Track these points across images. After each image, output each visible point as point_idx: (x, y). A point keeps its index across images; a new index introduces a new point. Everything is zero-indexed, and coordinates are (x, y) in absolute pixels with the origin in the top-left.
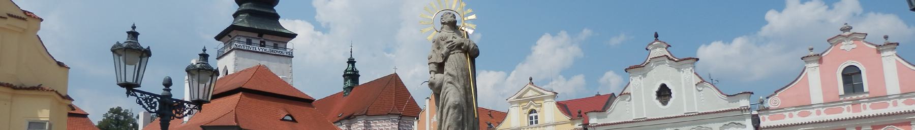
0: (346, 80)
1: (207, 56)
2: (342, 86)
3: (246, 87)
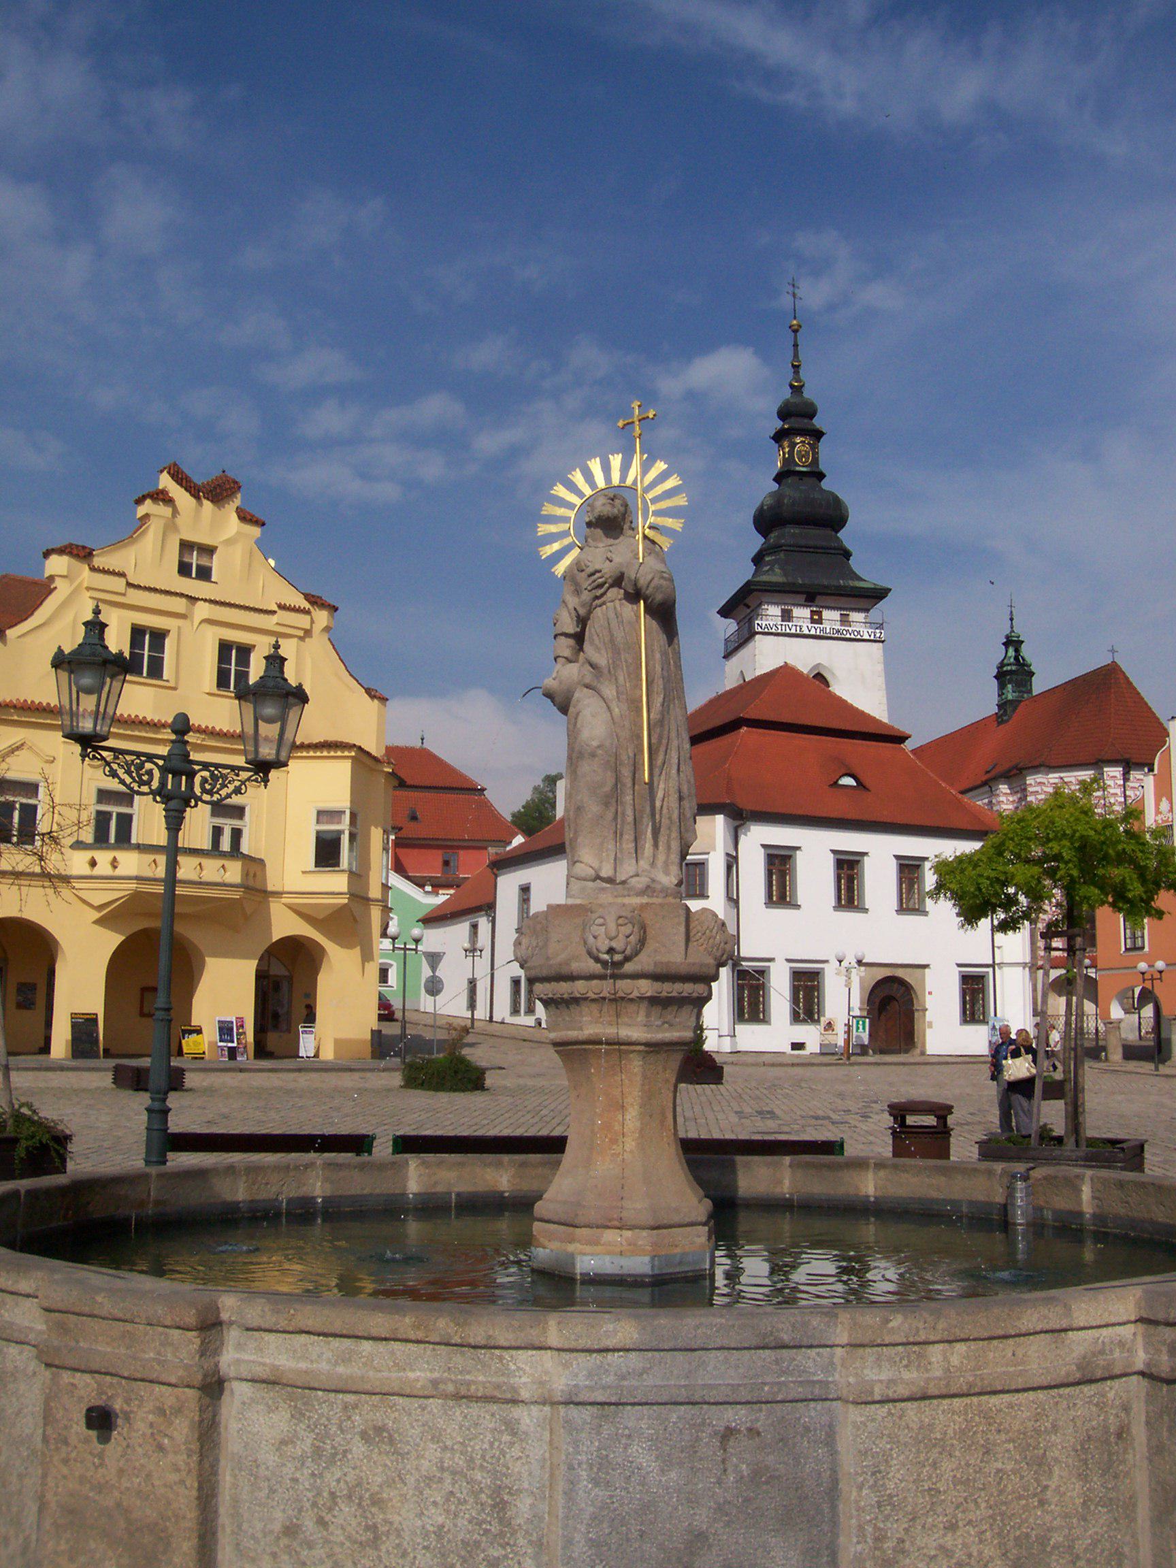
0: (1002, 686)
1: (283, 660)
2: (995, 700)
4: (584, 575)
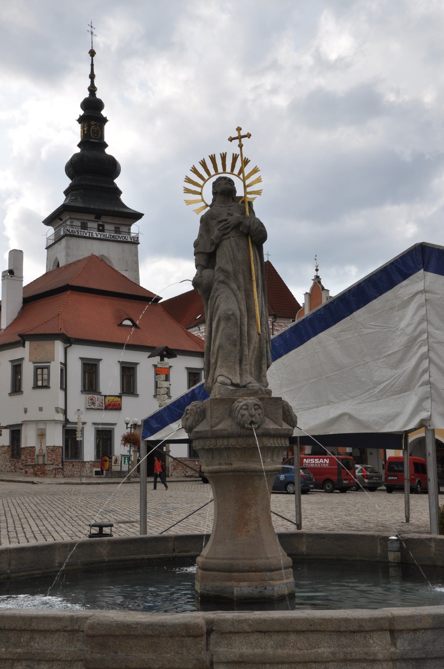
3: (75, 284)
4: (215, 222)
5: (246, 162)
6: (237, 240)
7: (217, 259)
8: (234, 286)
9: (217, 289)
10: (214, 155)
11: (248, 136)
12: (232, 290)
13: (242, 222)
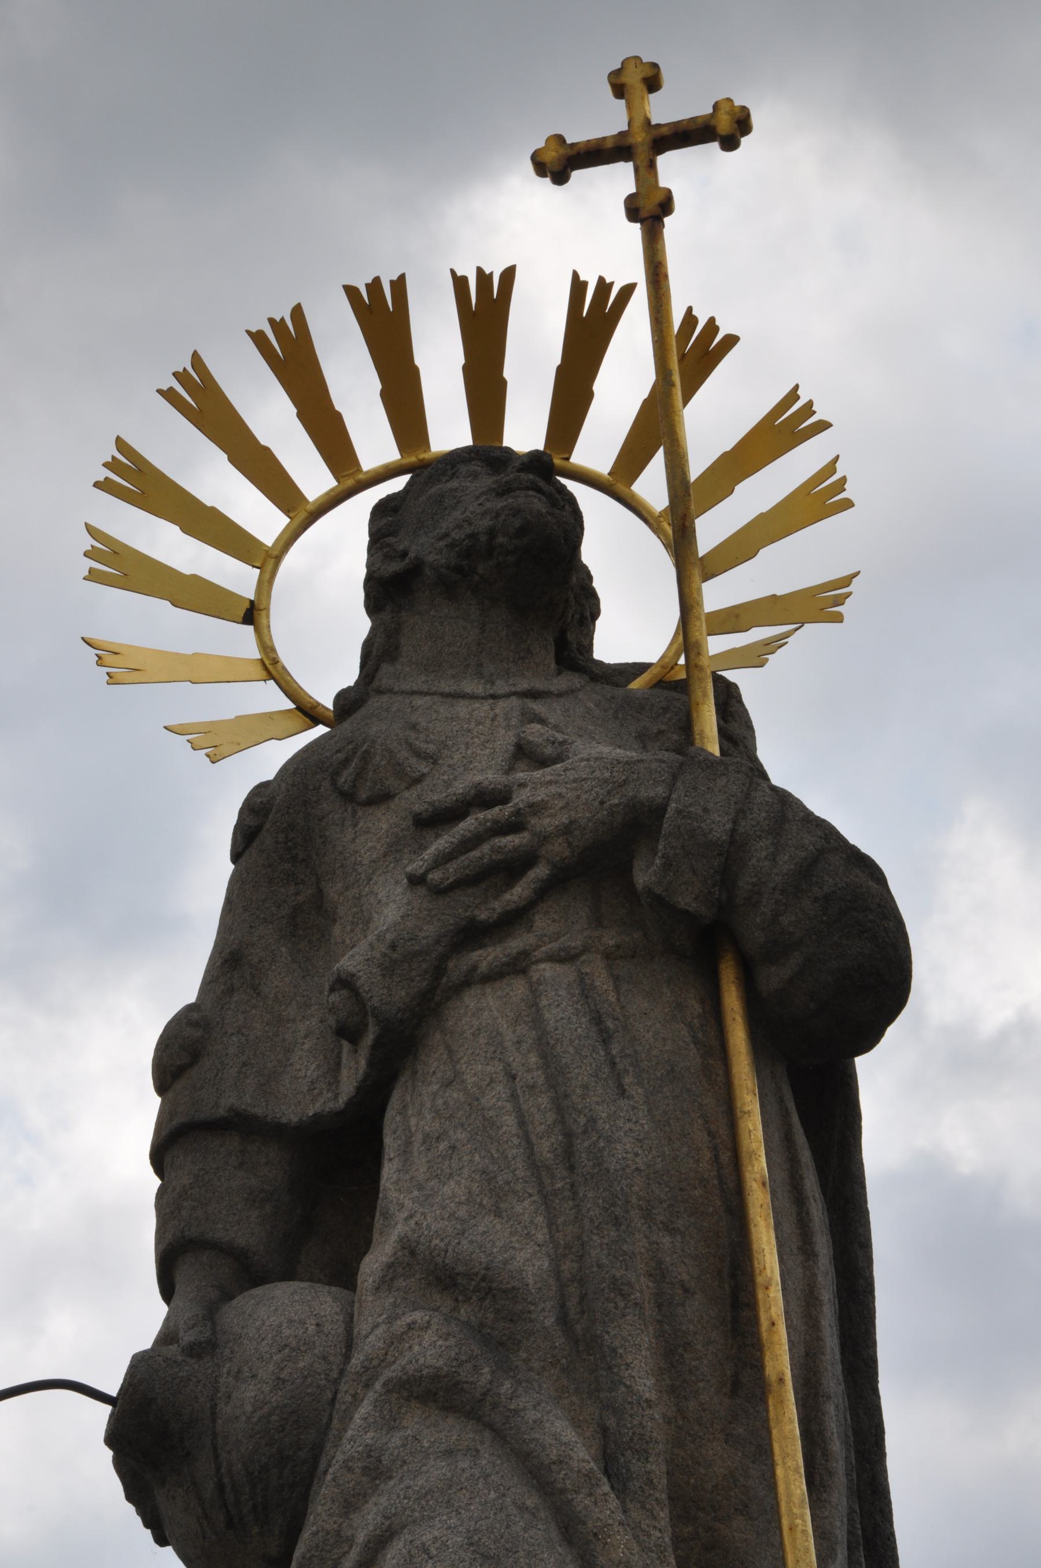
5: (692, 354)
6: (601, 980)
7: (389, 1171)
8: (562, 1435)
9: (376, 1470)
10: (399, 285)
11: (724, 124)
12: (537, 1472)
13: (658, 811)
